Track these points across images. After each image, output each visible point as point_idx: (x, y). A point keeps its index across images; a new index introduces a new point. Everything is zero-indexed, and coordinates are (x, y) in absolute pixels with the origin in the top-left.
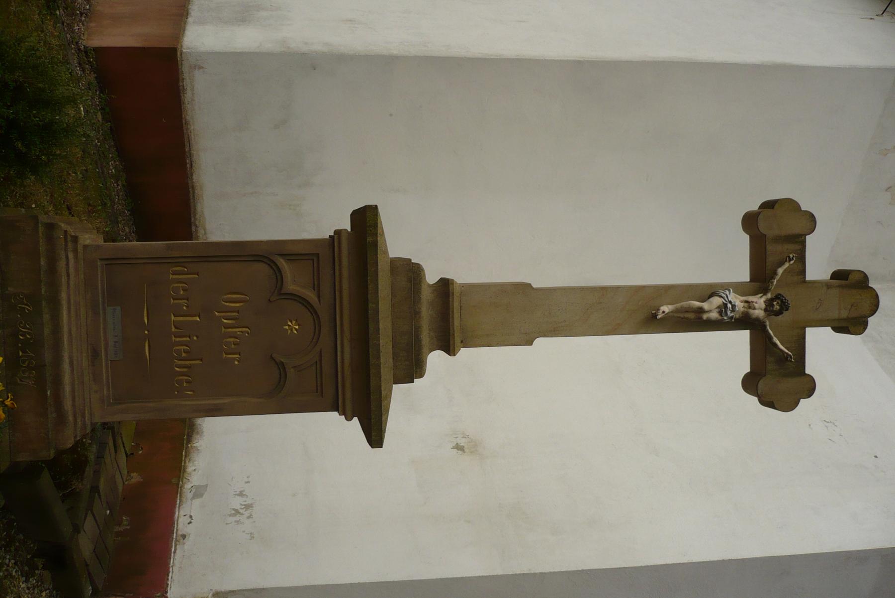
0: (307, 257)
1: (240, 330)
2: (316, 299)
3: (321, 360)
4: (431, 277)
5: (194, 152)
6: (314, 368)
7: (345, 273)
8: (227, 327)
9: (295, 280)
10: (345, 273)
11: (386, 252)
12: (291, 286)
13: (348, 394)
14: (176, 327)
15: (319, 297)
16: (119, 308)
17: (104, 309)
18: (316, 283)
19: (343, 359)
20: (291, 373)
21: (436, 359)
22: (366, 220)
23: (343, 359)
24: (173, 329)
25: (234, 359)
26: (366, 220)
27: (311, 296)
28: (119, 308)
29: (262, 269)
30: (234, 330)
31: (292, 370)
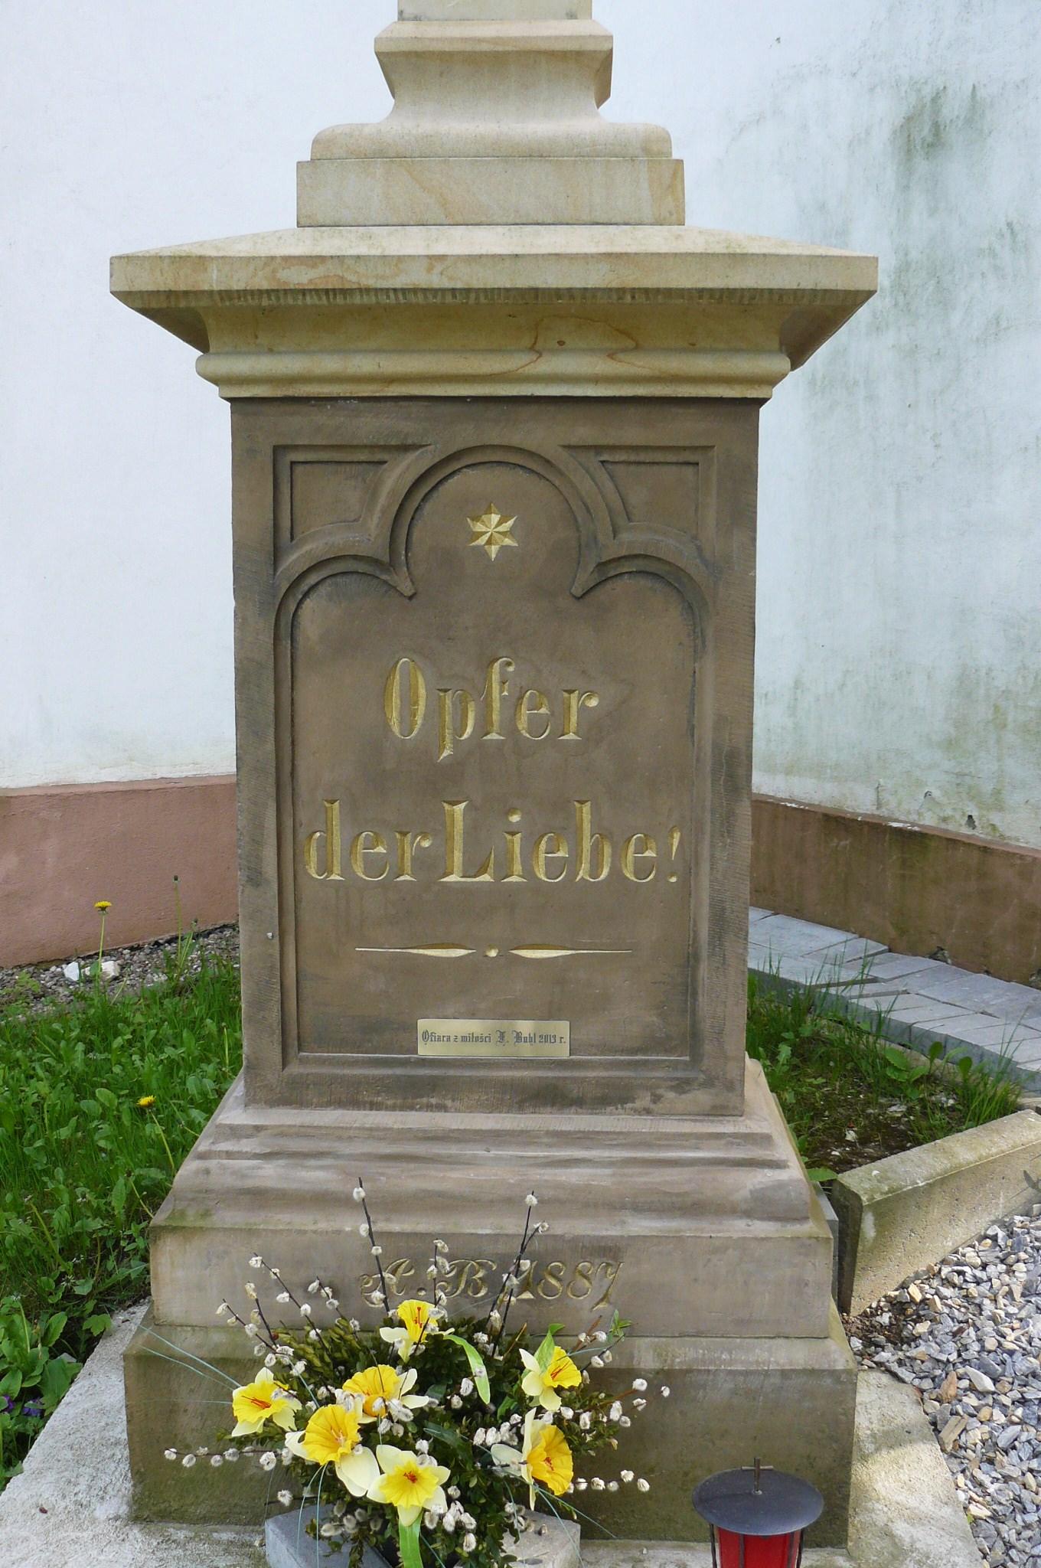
0: (285, 489)
1: (496, 687)
2: (411, 456)
3: (598, 449)
4: (368, 104)
5: (202, 778)
6: (620, 470)
7: (330, 364)
8: (484, 725)
9: (344, 518)
10: (330, 364)
11: (278, 235)
12: (368, 534)
13: (704, 364)
14: (482, 870)
15: (405, 448)
16: (423, 1024)
17: (424, 1062)
18: (363, 456)
19: (596, 380)
20: (632, 539)
21: (628, 108)
22: (187, 307)
23: (596, 380)
24: (486, 878)
25: (583, 709)
26: (187, 307)
27: (399, 473)
28: (423, 1024)
29: (316, 617)
30: (496, 705)
31: (625, 536)
